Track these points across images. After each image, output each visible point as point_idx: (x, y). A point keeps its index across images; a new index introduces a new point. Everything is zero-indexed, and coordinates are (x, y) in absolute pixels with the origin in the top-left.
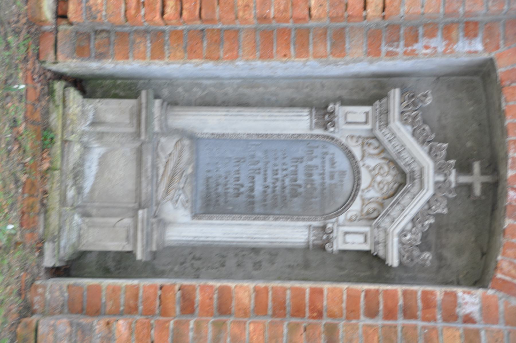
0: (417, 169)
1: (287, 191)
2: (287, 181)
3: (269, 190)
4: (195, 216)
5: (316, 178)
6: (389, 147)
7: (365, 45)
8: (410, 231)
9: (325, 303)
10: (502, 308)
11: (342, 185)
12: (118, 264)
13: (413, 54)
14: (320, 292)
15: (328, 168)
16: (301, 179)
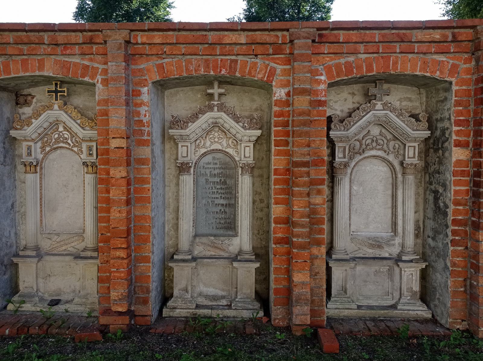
0: (211, 120)
1: (223, 187)
2: (218, 187)
3: (223, 196)
4: (236, 235)
5: (216, 172)
6: (200, 135)
7: (143, 147)
8: (243, 124)
9: (282, 167)
10: (282, 78)
11: (220, 158)
12: (263, 276)
13: (150, 124)
14: (276, 170)
15: (211, 166)
16: (217, 179)
